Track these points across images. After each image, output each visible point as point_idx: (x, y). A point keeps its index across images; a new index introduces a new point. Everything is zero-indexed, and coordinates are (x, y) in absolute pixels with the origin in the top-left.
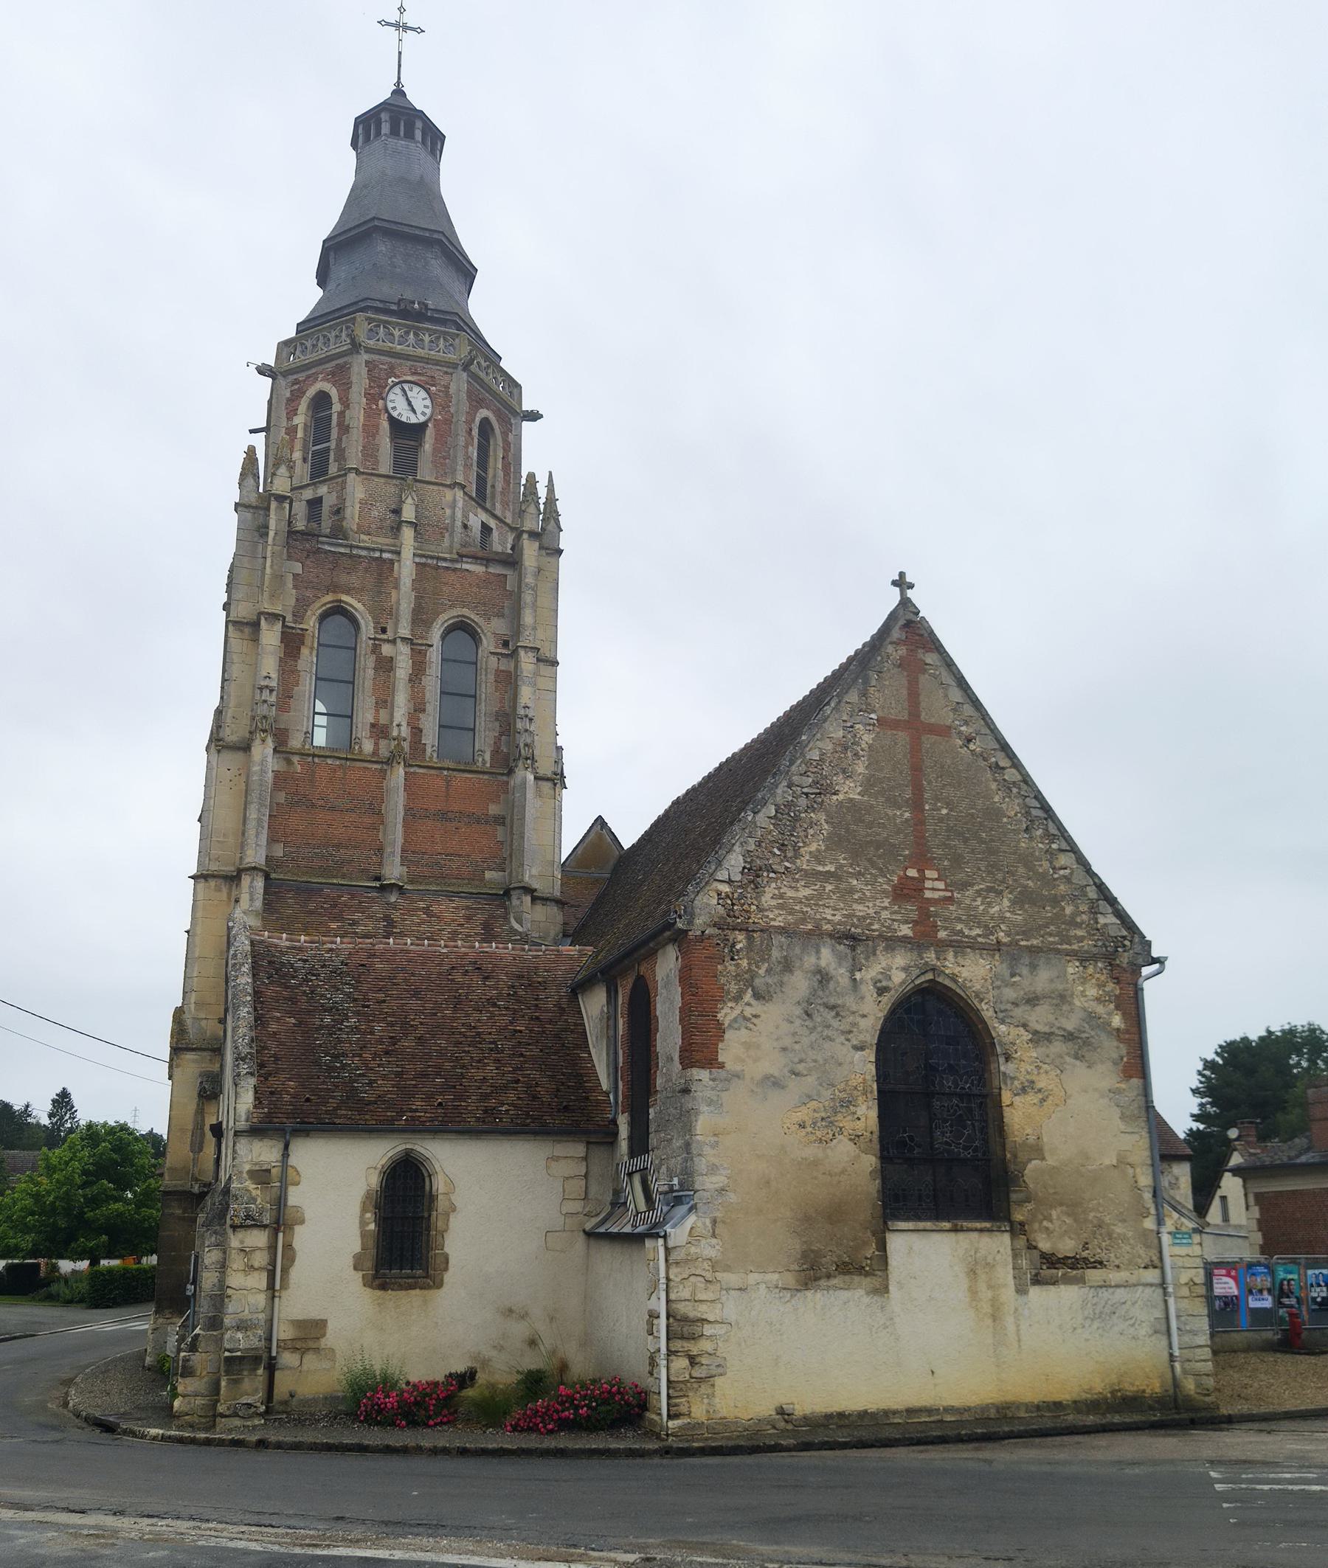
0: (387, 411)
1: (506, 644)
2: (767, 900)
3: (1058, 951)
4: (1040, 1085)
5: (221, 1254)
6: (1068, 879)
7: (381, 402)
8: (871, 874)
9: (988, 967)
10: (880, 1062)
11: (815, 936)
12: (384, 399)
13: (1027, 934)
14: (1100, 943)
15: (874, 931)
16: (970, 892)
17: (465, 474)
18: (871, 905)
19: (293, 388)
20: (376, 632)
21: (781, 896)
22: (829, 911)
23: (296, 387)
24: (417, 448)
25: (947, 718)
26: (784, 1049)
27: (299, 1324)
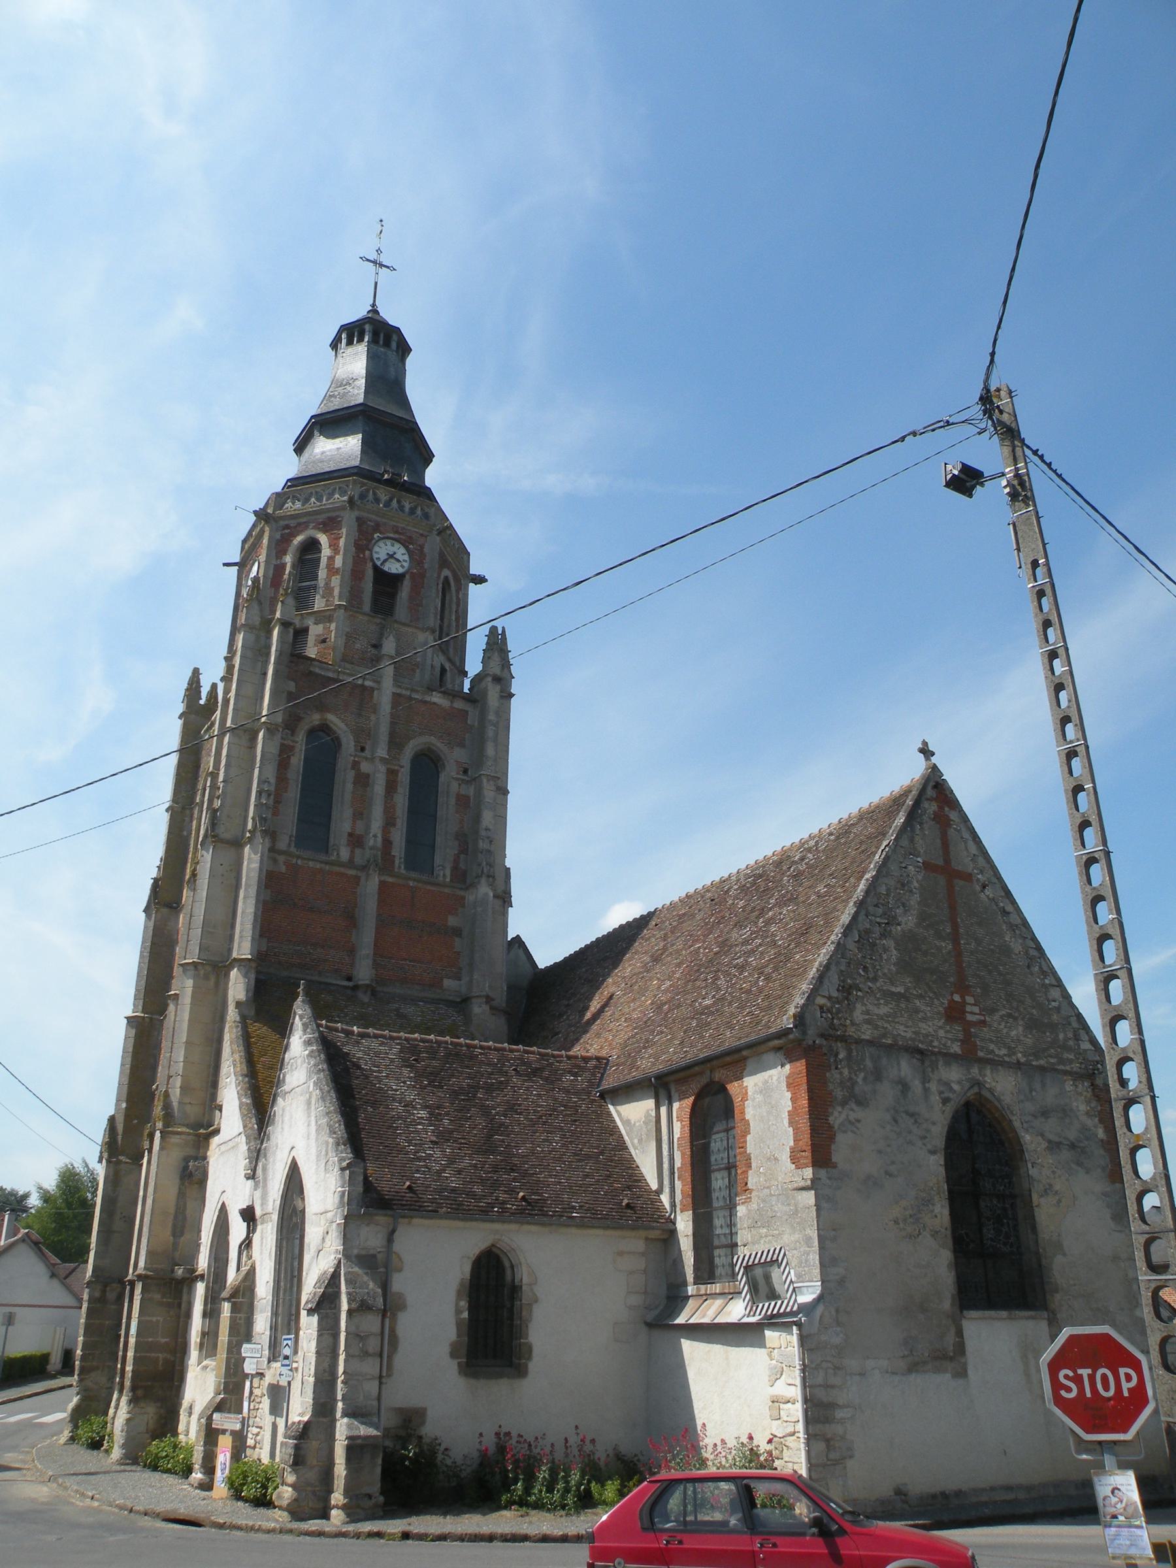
0: (372, 560)
1: (465, 771)
2: (858, 1015)
3: (1056, 1070)
4: (1057, 1187)
5: (331, 1339)
6: (1058, 1009)
7: (367, 553)
8: (929, 997)
9: (1014, 1083)
10: (949, 1165)
11: (895, 1049)
12: (371, 550)
13: (1037, 1056)
14: (1083, 1066)
15: (935, 1047)
16: (996, 1017)
17: (432, 621)
18: (930, 1024)
19: (283, 532)
20: (356, 750)
21: (867, 1012)
22: (902, 1028)
23: (287, 531)
24: (393, 596)
25: (970, 868)
26: (880, 1152)
27: (400, 1411)
